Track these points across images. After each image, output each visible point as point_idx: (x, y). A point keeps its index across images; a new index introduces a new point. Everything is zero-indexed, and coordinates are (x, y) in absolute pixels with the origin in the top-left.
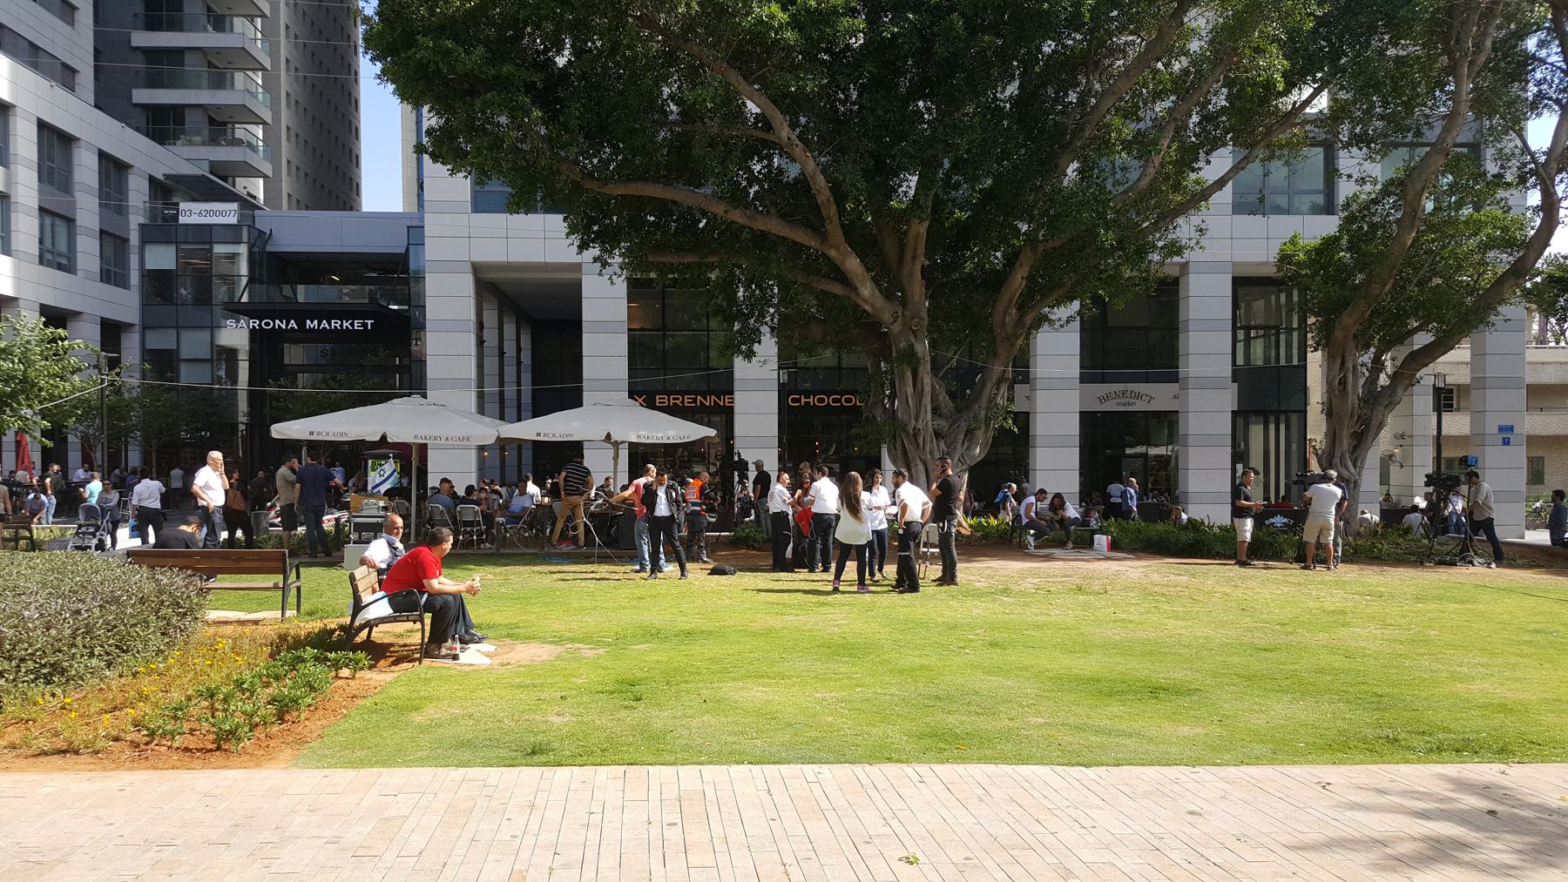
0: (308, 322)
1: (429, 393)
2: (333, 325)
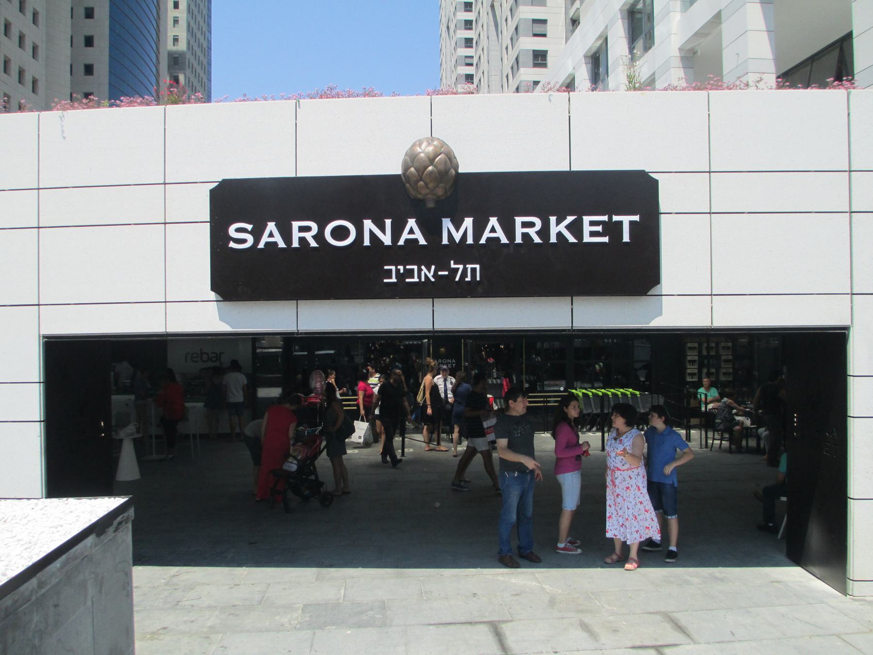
0: (447, 224)
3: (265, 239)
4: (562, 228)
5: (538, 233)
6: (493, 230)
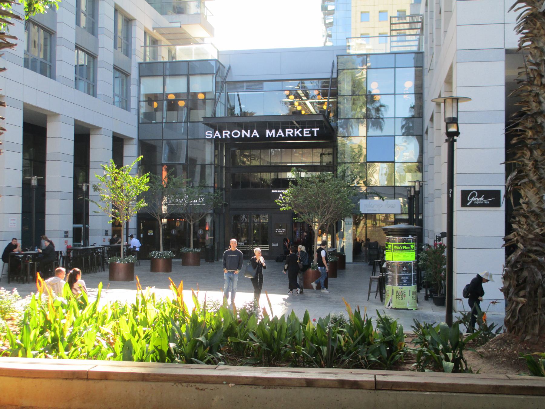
0: (268, 131)
1: (328, 288)
2: (224, 134)
4: (298, 132)
5: (229, 135)
6: (280, 133)
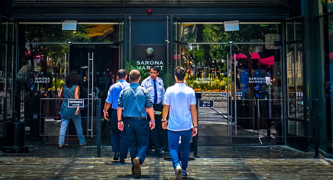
3: (142, 63)
4: (259, 82)
